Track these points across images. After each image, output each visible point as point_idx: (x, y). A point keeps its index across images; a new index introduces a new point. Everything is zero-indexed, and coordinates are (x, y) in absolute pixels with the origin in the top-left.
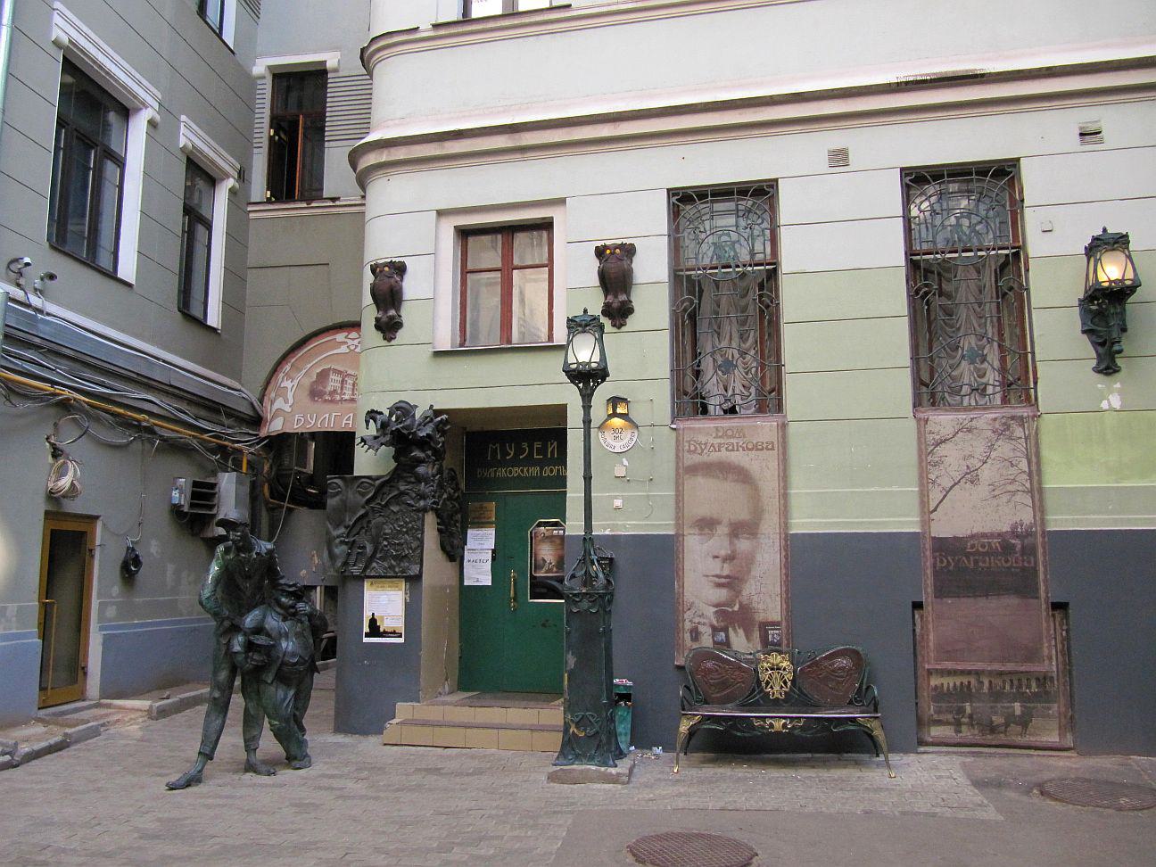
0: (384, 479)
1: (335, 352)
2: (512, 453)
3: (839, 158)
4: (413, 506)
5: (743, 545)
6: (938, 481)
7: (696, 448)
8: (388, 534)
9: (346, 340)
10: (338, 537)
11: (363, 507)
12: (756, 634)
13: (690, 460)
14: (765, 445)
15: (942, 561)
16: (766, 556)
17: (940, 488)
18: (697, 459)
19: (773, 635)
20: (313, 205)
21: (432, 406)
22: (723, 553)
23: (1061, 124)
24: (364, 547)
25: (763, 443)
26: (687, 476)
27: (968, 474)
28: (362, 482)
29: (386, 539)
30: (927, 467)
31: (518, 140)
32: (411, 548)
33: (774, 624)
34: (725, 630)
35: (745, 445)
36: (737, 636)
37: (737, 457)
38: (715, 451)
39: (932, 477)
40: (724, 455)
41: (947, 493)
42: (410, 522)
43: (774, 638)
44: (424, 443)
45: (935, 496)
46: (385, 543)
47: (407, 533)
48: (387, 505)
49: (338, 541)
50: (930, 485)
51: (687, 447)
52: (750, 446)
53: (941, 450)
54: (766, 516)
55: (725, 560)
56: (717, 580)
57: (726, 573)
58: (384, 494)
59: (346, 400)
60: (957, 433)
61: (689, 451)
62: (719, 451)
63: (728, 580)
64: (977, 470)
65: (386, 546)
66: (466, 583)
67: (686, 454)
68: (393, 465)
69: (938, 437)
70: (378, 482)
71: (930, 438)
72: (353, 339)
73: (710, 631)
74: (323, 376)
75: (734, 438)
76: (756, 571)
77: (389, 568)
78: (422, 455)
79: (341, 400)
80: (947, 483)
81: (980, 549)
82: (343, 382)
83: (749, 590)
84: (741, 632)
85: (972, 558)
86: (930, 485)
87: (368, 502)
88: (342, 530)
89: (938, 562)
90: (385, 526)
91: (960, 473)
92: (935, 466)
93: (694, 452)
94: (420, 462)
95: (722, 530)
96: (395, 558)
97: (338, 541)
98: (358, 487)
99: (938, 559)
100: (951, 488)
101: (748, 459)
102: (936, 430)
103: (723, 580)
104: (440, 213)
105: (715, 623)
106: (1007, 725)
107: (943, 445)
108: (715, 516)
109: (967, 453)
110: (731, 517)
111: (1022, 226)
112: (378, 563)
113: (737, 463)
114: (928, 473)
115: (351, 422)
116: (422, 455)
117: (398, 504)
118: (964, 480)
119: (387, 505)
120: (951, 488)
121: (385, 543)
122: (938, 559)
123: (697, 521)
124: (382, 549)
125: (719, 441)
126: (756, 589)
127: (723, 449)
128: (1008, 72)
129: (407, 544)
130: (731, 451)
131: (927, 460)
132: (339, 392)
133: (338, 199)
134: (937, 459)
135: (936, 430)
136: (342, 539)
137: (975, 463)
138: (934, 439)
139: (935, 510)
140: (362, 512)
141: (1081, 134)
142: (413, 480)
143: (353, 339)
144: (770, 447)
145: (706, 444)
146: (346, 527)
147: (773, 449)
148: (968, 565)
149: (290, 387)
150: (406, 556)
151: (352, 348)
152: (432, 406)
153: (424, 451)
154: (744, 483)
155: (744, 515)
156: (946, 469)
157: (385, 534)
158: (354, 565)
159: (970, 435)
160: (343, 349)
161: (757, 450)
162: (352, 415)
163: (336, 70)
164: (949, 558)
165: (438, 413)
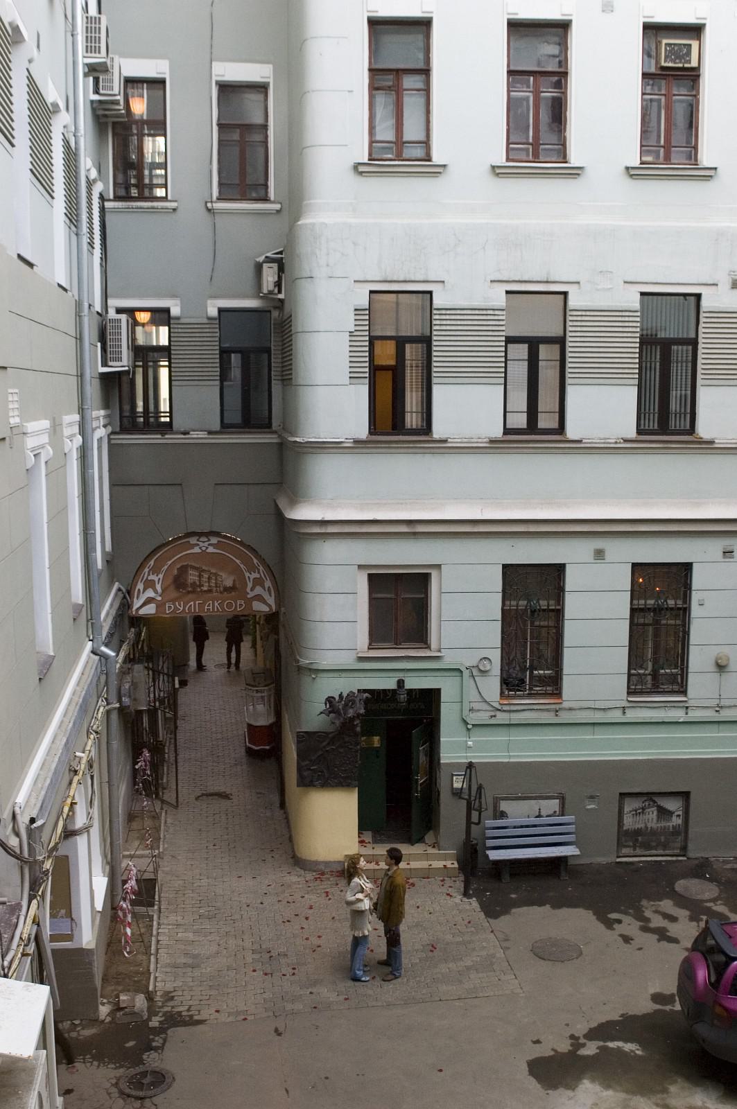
1: (188, 552)
2: (390, 695)
3: (599, 554)
9: (198, 543)
20: (167, 436)
23: (714, 548)
29: (336, 767)
31: (413, 530)
47: (350, 764)
49: (305, 768)
59: (205, 591)
70: (330, 736)
72: (204, 542)
74: (183, 570)
79: (201, 591)
82: (200, 576)
104: (360, 567)
106: (657, 846)
111: (696, 448)
115: (211, 608)
128: (697, 359)
132: (198, 583)
133: (188, 433)
140: (320, 753)
141: (724, 552)
142: (352, 734)
143: (204, 542)
146: (311, 761)
149: (156, 579)
151: (204, 549)
160: (197, 550)
162: (211, 602)
163: (178, 318)
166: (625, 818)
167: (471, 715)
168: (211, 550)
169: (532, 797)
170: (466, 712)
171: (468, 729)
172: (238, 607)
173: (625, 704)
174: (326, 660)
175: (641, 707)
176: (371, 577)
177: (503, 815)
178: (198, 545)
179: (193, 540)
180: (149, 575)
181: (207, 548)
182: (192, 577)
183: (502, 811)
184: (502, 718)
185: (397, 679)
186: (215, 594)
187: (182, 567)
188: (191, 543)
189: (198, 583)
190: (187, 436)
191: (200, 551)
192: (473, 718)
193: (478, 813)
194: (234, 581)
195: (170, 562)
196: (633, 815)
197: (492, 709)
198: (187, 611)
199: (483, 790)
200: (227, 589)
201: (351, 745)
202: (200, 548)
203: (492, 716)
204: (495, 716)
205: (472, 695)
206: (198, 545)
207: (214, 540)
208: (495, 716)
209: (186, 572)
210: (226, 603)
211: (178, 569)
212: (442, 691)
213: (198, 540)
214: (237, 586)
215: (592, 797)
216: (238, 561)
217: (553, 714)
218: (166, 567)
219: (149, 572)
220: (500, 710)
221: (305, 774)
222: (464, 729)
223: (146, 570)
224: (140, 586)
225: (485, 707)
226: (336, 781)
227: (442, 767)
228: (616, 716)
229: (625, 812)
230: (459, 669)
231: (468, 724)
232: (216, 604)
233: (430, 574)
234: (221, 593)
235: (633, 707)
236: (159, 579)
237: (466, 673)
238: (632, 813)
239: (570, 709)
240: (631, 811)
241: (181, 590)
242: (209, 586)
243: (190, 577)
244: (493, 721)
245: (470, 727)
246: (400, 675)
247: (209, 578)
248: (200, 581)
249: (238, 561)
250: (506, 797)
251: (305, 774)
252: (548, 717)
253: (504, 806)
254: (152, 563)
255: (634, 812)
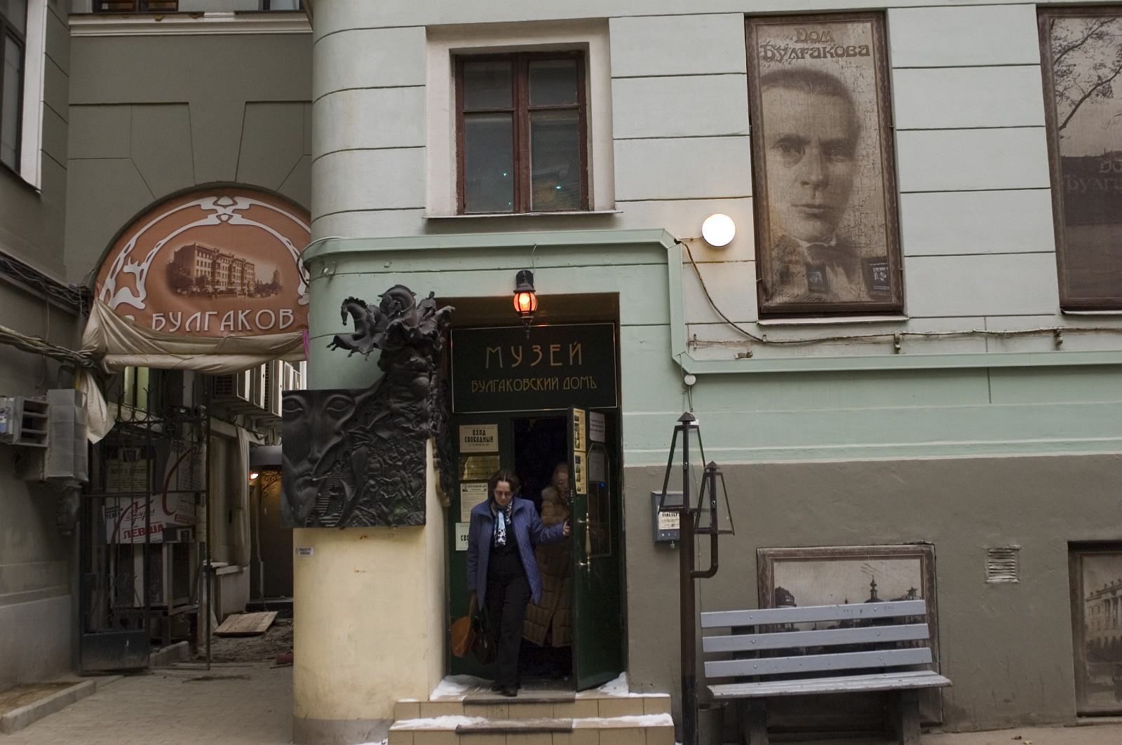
0: (369, 393)
4: (413, 431)
5: (839, 168)
6: (1067, 94)
7: (774, 55)
8: (376, 470)
10: (302, 475)
11: (338, 434)
12: (859, 276)
13: (766, 68)
14: (857, 50)
15: (1073, 185)
16: (866, 181)
17: (1069, 102)
18: (775, 66)
19: (879, 273)
21: (432, 293)
22: (813, 178)
24: (341, 489)
25: (855, 48)
26: (765, 87)
27: (1099, 85)
28: (335, 399)
29: (372, 477)
30: (1053, 78)
32: (411, 489)
33: (878, 260)
34: (822, 269)
35: (833, 51)
36: (836, 276)
37: (829, 65)
38: (798, 58)
39: (1060, 88)
40: (808, 62)
41: (1077, 106)
42: (408, 453)
43: (880, 276)
44: (421, 344)
45: (1063, 109)
46: (372, 482)
48: (373, 430)
49: (301, 480)
50: (1058, 99)
51: (763, 54)
52: (840, 52)
53: (1070, 58)
54: (863, 134)
55: (817, 186)
56: (807, 209)
57: (818, 201)
58: (366, 414)
59: (221, 292)
60: (1086, 39)
61: (765, 58)
62: (803, 57)
63: (821, 210)
64: (1109, 81)
65: (373, 486)
66: (497, 450)
67: (762, 62)
68: (378, 374)
69: (1065, 43)
70: (358, 399)
71: (1056, 44)
72: (225, 207)
73: (803, 270)
74: (185, 255)
75: (819, 42)
76: (855, 200)
77: (379, 516)
78: (422, 360)
80: (1076, 95)
81: (1115, 170)
82: (214, 265)
83: (848, 218)
84: (840, 270)
85: (1106, 180)
86: (1058, 99)
87: (345, 425)
88: (306, 465)
89: (1069, 186)
90: (370, 459)
91: (1091, 84)
92: (1063, 76)
93: (772, 58)
94: (421, 369)
95: (812, 151)
96: (387, 502)
97: (301, 480)
98: (329, 405)
99: (1069, 182)
100: (1081, 101)
101: (838, 67)
102: (1063, 36)
103: (816, 211)
105: (810, 260)
107: (1071, 53)
108: (802, 135)
109: (1098, 61)
110: (821, 136)
111: (998, 445)
112: (361, 510)
113: (825, 71)
114: (1055, 85)
115: (231, 323)
116: (422, 360)
117: (388, 428)
118: (1095, 92)
119: (373, 430)
120: (1081, 101)
121: (372, 482)
122: (1069, 182)
123: (782, 140)
124: (368, 491)
125: (800, 45)
126: (855, 220)
127: (807, 56)
129: (404, 483)
130: (816, 57)
131: (1053, 69)
132: (210, 279)
133: (201, 14)
134: (1064, 68)
135: (1063, 36)
136: (307, 478)
137: (1106, 73)
138: (1060, 45)
139: (1064, 126)
140: (335, 440)
142: (409, 395)
143: (225, 207)
144: (864, 51)
145: (786, 49)
146: (313, 461)
147: (867, 54)
148: (1102, 188)
150: (404, 498)
151: (224, 218)
152: (432, 293)
153: (423, 356)
154: (834, 95)
155: (836, 133)
156: (1075, 79)
157: (371, 470)
158: (326, 514)
159: (1101, 43)
160: (212, 220)
161: (848, 55)
164: (1081, 180)
165: (441, 302)
166: (1087, 611)
167: (692, 354)
168: (237, 220)
169: (850, 552)
170: (679, 346)
171: (688, 388)
172: (281, 323)
173: (1057, 322)
174: (350, 231)
175: (1096, 330)
176: (460, 62)
177: (782, 598)
178: (215, 211)
179: (207, 203)
180: (125, 263)
181: (230, 217)
182: (199, 268)
183: (779, 589)
184: (764, 360)
185: (517, 272)
186: (239, 297)
187: (183, 249)
188: (203, 208)
189: (210, 279)
190: (200, 20)
191: (217, 222)
192: (697, 362)
193: (708, 537)
194: (276, 274)
195: (163, 242)
196: (1107, 601)
197: (743, 340)
198: (188, 330)
199: (718, 478)
200: (262, 289)
201: (409, 421)
202: (219, 217)
203: (741, 356)
204: (749, 355)
205: (688, 306)
206: (215, 211)
207: (244, 203)
208: (749, 355)
209: (192, 258)
210: (261, 312)
211: (175, 252)
212: (620, 295)
213: (215, 203)
214: (281, 283)
215: (1000, 554)
216: (284, 240)
217: (886, 351)
218: (155, 250)
219: (126, 258)
220: (759, 342)
221: (302, 494)
222: (676, 387)
223: (122, 255)
224: (110, 283)
225: (723, 333)
226: (372, 511)
227: (626, 474)
228: (1039, 352)
229: (1087, 595)
230: (658, 245)
231: (686, 373)
232: (241, 317)
233: (587, 44)
234: (250, 295)
235: (1078, 330)
236: (142, 270)
237: (675, 254)
238: (1104, 597)
239: (928, 337)
240: (1100, 593)
241: (179, 291)
242: (230, 283)
243: (197, 267)
244: (745, 367)
245: (690, 380)
246: (523, 263)
247: (230, 269)
248: (213, 274)
249: (284, 240)
250: (785, 554)
251: (302, 494)
252: (879, 358)
253: (784, 576)
254: (132, 242)
255: (1110, 596)
